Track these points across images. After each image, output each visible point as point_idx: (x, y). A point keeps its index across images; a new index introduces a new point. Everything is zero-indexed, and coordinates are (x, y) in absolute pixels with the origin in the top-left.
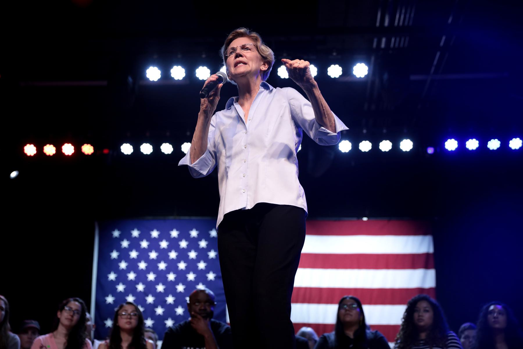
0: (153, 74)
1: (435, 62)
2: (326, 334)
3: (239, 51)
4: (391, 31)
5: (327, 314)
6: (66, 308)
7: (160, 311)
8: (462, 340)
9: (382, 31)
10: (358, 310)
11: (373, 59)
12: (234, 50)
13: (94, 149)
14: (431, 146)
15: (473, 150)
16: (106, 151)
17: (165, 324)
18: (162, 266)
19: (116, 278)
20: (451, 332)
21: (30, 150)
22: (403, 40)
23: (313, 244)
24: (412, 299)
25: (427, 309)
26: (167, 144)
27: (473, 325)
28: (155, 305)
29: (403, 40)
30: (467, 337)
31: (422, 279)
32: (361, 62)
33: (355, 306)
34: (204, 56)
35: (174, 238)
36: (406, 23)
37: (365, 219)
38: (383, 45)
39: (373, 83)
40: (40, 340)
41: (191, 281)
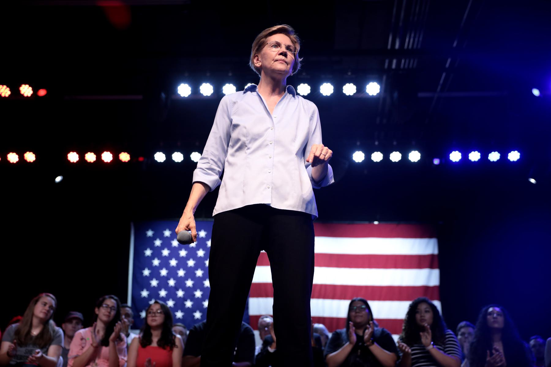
0: (184, 90)
1: (441, 82)
2: (338, 331)
3: (283, 49)
4: (401, 53)
5: (339, 309)
6: (104, 306)
7: (189, 304)
8: (459, 337)
9: (393, 53)
10: (367, 311)
11: (384, 78)
12: (278, 45)
13: (131, 157)
14: (437, 157)
15: (178, 163)
16: (141, 159)
17: (194, 316)
18: (180, 293)
19: (150, 274)
20: (449, 330)
21: (73, 157)
22: (412, 61)
23: (323, 245)
24: (418, 297)
25: (427, 309)
26: (515, 160)
27: (468, 323)
28: (184, 299)
29: (412, 61)
30: (463, 334)
31: (428, 277)
32: (327, 82)
33: (364, 307)
34: (230, 74)
35: (167, 237)
36: (415, 46)
37: (376, 223)
38: (394, 66)
39: (384, 99)
40: (80, 333)
41: (187, 264)
